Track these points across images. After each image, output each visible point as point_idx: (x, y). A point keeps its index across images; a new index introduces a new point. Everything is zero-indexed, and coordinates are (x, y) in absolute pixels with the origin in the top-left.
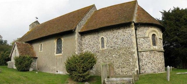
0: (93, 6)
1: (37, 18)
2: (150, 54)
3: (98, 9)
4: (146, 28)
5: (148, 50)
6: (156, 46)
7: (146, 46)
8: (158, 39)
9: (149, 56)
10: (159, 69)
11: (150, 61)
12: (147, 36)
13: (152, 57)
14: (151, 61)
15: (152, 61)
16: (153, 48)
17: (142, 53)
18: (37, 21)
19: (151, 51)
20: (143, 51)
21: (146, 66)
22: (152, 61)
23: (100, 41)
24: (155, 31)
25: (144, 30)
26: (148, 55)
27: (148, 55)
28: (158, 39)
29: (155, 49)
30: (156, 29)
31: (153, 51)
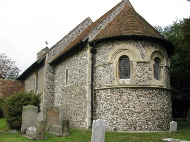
0: (88, 19)
1: (47, 43)
2: (112, 94)
3: (93, 21)
4: (109, 47)
5: (109, 86)
6: (129, 78)
7: (105, 80)
8: (135, 64)
9: (109, 98)
10: (133, 125)
11: (110, 107)
12: (108, 61)
13: (114, 100)
14: (112, 107)
15: (115, 107)
16: (117, 84)
17: (100, 91)
18: (47, 47)
19: (113, 89)
20: (103, 89)
21: (104, 116)
22: (115, 107)
23: (66, 71)
24: (123, 50)
25: (106, 50)
26: (108, 96)
27: (108, 96)
28: (135, 64)
29: (121, 85)
30: (123, 45)
31: (117, 88)
